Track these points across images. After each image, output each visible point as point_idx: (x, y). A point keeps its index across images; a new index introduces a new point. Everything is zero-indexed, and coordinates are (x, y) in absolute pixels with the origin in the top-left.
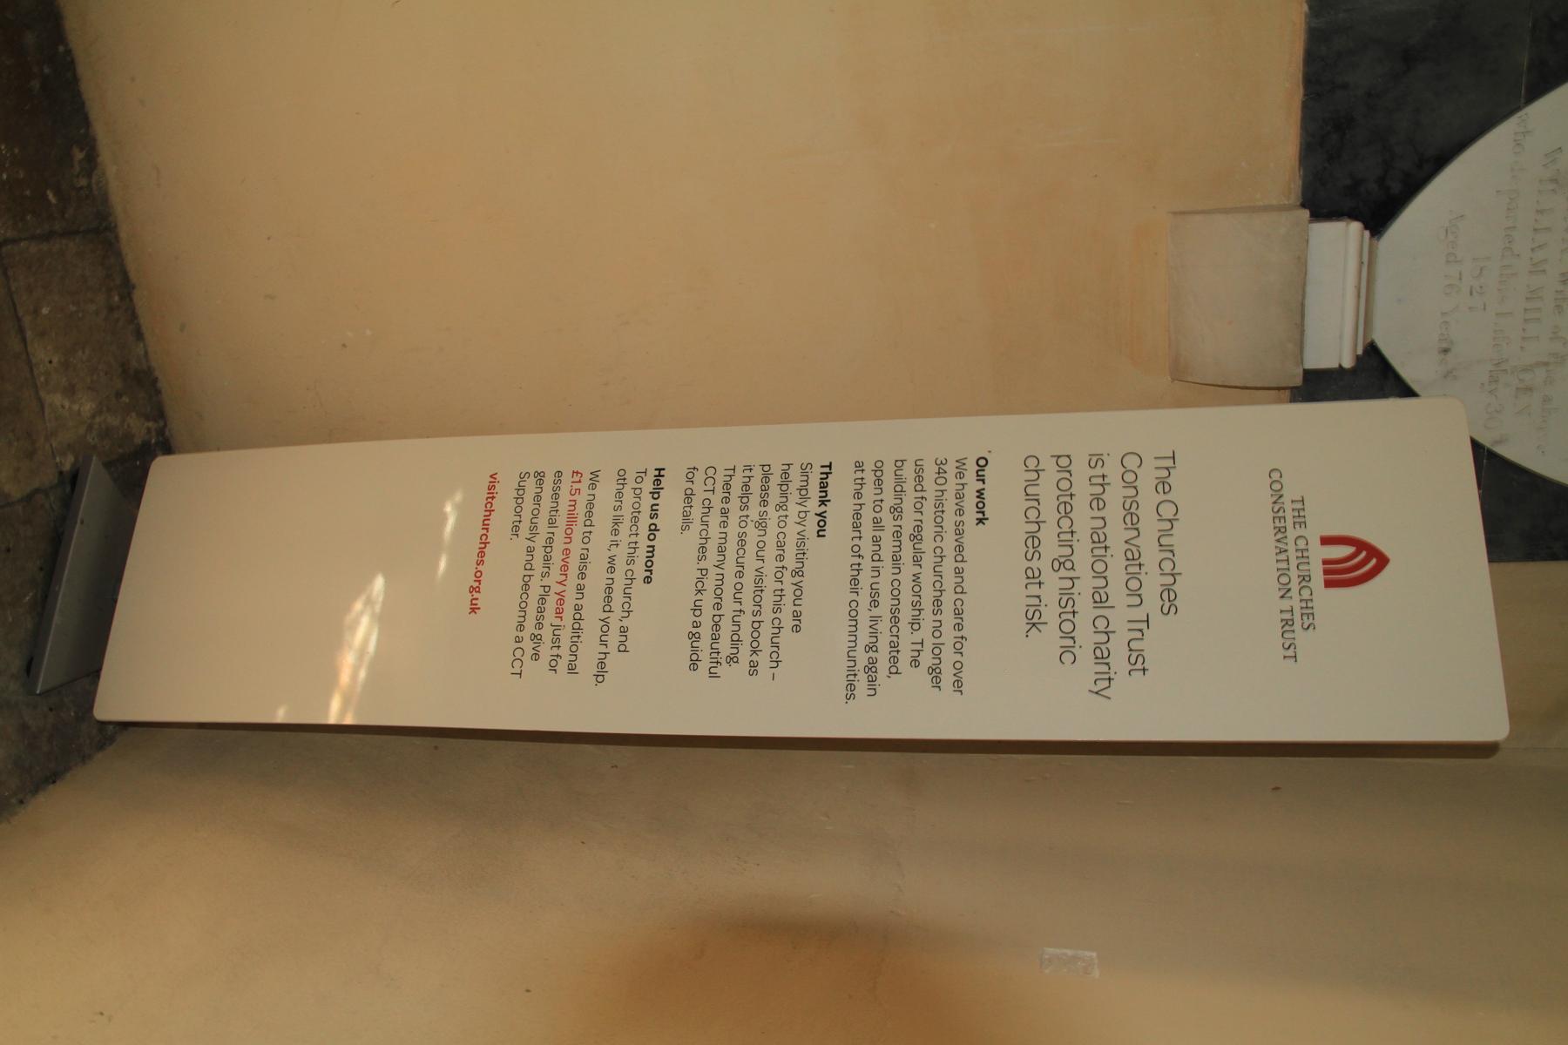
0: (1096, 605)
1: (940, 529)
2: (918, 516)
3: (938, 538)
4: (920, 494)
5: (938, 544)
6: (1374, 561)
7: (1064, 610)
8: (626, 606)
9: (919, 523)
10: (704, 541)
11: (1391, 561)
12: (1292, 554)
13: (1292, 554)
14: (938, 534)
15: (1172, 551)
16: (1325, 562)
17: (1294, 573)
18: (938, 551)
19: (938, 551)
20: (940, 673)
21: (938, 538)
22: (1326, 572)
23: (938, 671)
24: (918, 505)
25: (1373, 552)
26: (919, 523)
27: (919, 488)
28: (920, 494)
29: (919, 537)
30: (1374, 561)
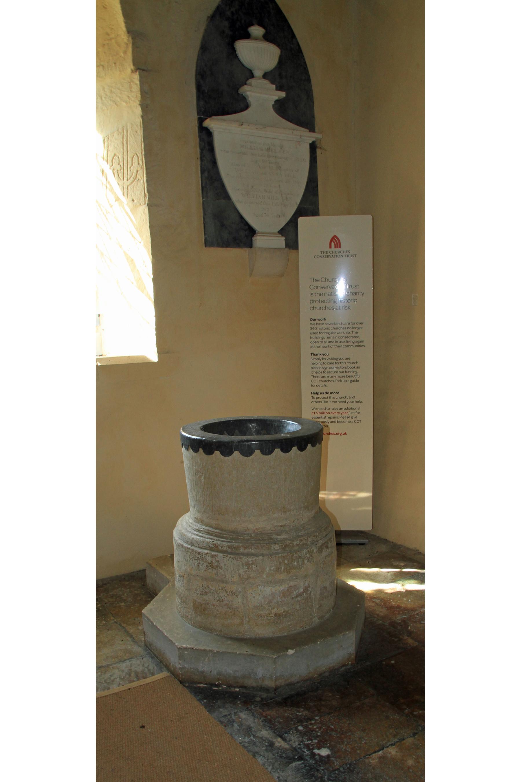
3: (329, 329)
12: (333, 254)
14: (328, 329)
16: (335, 248)
21: (329, 329)
22: (337, 248)
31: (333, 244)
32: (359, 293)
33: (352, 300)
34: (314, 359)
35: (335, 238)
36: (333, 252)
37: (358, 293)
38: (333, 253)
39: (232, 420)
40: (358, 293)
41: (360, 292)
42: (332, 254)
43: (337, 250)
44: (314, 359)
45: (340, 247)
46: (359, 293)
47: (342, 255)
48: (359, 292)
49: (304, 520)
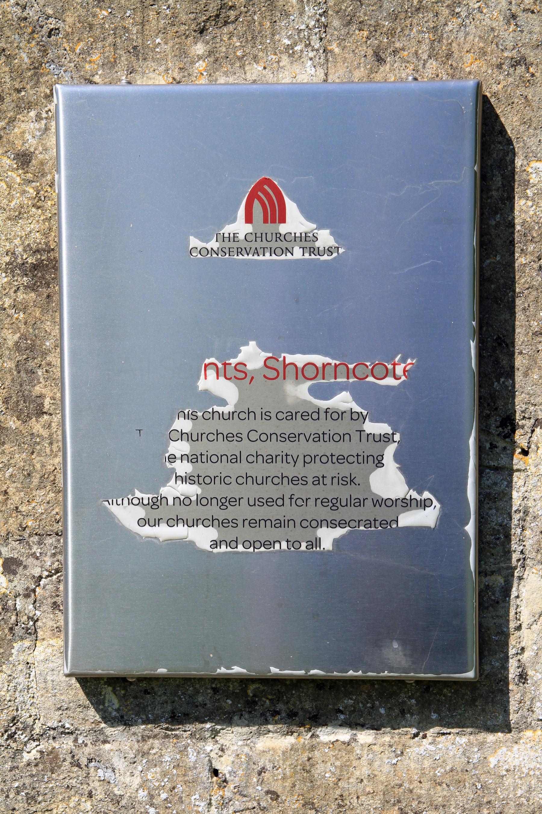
0: (239, 461)
1: (218, 479)
2: (311, 502)
3: (227, 480)
4: (287, 501)
5: (233, 480)
6: (266, 187)
7: (219, 501)
8: (211, 437)
9: (319, 501)
10: (220, 436)
11: (242, 352)
12: (259, 244)
13: (259, 244)
14: (223, 480)
15: (233, 413)
16: (265, 221)
17: (274, 244)
18: (240, 480)
19: (240, 480)
20: (226, 498)
21: (227, 480)
22: (273, 221)
23: (223, 500)
24: (299, 502)
25: (259, 186)
26: (319, 501)
27: (280, 502)
28: (287, 501)
29: (334, 501)
30: (266, 187)
31: (257, 206)
32: (284, 457)
33: (218, 479)
34: (262, 522)
35: (259, 193)
36: (259, 235)
37: (279, 458)
38: (259, 240)
39: (162, 671)
40: (279, 458)
41: (287, 455)
42: (254, 245)
43: (269, 228)
44: (262, 522)
45: (283, 220)
46: (284, 457)
47: (289, 246)
48: (284, 454)
49: (21, 142)
